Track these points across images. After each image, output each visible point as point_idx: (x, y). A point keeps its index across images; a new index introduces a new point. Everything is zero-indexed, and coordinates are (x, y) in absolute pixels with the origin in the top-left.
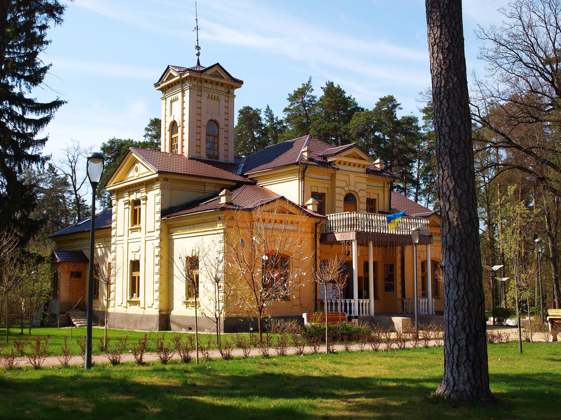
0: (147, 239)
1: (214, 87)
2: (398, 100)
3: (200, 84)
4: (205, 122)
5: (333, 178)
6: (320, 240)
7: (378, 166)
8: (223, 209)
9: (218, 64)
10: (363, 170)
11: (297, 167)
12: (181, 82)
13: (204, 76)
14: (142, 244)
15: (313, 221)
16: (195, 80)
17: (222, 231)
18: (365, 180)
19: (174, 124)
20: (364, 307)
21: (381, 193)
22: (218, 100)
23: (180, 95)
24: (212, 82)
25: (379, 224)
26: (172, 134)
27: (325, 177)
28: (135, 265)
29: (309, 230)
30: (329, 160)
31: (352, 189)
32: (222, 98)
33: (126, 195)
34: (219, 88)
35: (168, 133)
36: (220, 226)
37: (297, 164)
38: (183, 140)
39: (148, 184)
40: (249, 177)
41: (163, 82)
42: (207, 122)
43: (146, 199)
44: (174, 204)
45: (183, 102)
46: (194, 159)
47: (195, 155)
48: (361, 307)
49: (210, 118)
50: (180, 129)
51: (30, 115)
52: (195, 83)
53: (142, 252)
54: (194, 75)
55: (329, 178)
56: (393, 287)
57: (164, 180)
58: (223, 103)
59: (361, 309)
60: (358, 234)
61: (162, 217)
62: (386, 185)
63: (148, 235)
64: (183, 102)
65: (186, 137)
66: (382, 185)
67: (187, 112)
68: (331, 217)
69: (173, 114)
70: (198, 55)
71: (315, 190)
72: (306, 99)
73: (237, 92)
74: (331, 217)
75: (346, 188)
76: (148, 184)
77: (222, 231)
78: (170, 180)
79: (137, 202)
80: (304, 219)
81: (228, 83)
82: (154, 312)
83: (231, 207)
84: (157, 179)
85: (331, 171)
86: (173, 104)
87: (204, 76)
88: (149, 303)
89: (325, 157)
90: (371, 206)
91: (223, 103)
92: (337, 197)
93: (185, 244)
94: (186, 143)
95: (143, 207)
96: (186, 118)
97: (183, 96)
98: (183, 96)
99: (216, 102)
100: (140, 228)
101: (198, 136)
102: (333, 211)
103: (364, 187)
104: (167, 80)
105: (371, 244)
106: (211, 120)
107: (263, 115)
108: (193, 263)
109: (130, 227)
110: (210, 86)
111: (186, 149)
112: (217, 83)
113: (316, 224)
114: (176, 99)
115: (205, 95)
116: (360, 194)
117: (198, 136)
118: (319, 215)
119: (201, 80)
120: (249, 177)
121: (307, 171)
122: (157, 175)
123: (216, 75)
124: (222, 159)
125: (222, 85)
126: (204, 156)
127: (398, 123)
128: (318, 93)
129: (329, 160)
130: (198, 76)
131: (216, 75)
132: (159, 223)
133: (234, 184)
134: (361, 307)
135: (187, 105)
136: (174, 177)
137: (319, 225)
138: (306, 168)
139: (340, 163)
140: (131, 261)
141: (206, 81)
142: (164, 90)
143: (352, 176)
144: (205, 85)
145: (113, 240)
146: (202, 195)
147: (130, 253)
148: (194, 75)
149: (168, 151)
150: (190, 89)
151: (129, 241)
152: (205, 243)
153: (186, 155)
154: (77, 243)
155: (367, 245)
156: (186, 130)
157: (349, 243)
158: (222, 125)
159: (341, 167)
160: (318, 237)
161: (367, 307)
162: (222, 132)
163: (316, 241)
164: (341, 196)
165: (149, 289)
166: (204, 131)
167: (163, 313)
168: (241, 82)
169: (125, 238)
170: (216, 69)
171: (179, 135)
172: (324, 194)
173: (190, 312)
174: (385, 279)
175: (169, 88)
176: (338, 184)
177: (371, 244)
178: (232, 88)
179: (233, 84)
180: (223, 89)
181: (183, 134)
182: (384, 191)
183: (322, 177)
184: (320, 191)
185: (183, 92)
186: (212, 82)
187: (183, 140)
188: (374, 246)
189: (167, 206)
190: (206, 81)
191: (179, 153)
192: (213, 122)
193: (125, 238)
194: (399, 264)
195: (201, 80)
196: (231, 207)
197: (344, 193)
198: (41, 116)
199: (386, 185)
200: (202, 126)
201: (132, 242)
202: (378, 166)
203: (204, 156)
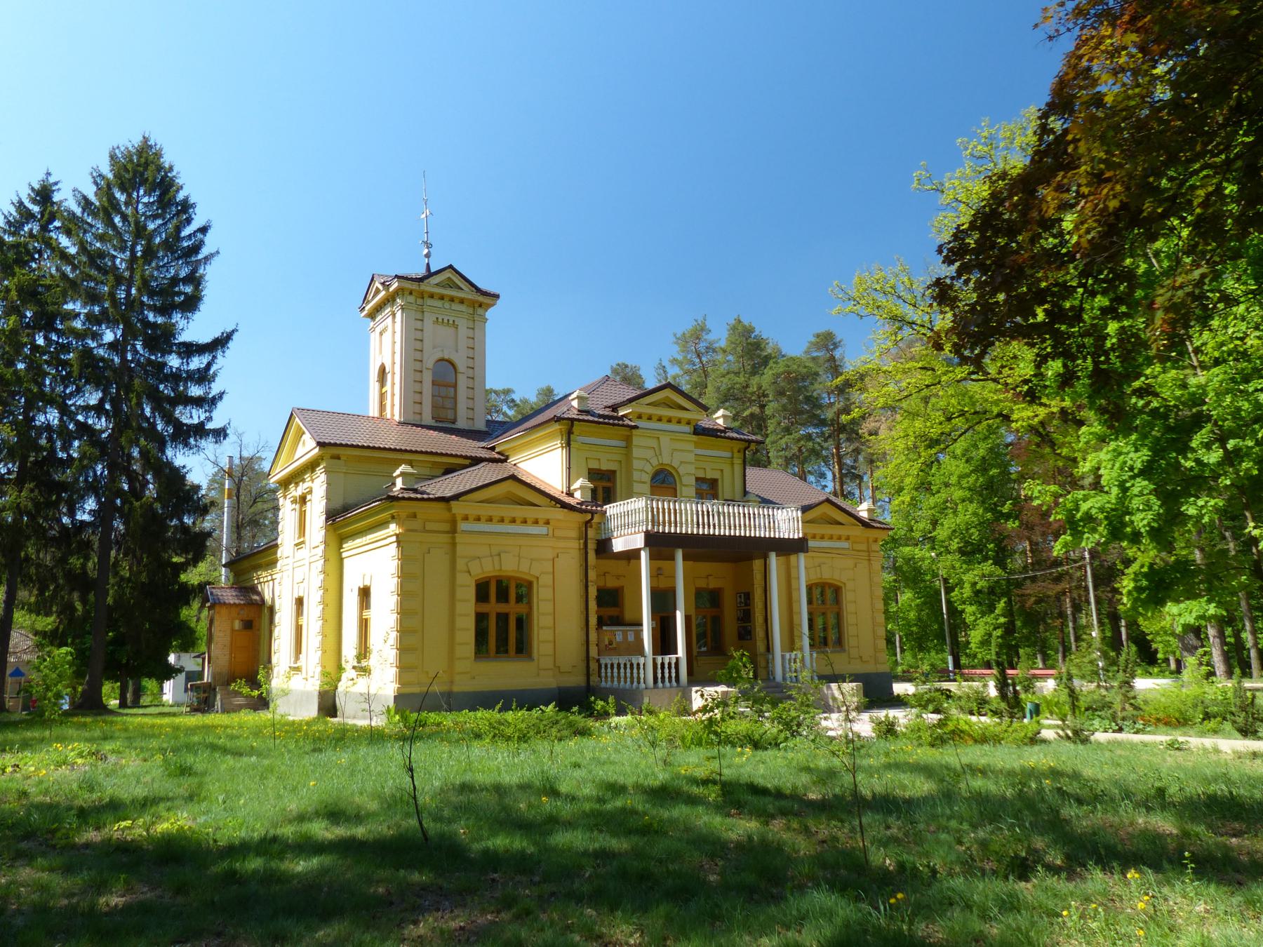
1: (447, 305)
2: (839, 335)
3: (420, 301)
4: (430, 363)
5: (628, 446)
7: (720, 421)
9: (451, 267)
10: (688, 429)
12: (389, 300)
18: (691, 447)
20: (666, 671)
24: (442, 298)
25: (689, 516)
30: (621, 414)
31: (666, 460)
32: (463, 324)
34: (456, 306)
36: (393, 528)
38: (393, 395)
41: (369, 302)
47: (411, 419)
48: (659, 671)
49: (438, 355)
52: (411, 299)
54: (408, 285)
55: (623, 444)
58: (463, 331)
59: (659, 675)
73: (490, 313)
75: (655, 462)
76: (311, 466)
77: (394, 539)
78: (343, 458)
83: (419, 496)
88: (310, 674)
91: (463, 331)
97: (394, 322)
98: (394, 322)
99: (451, 330)
101: (417, 387)
103: (691, 457)
105: (679, 554)
106: (442, 360)
110: (439, 303)
112: (452, 300)
116: (682, 470)
117: (417, 387)
123: (450, 284)
124: (461, 424)
125: (462, 301)
126: (428, 419)
128: (719, 335)
130: (414, 286)
131: (450, 284)
133: (467, 462)
134: (659, 671)
138: (572, 425)
139: (640, 417)
141: (432, 296)
143: (665, 440)
144: (429, 302)
147: (296, 586)
150: (402, 309)
155: (672, 558)
158: (461, 367)
161: (673, 671)
162: (462, 382)
163: (586, 553)
164: (644, 475)
166: (428, 378)
168: (497, 296)
170: (447, 274)
172: (614, 472)
176: (636, 452)
177: (679, 554)
178: (480, 306)
179: (481, 299)
180: (463, 308)
181: (393, 384)
183: (608, 442)
184: (605, 466)
185: (394, 315)
186: (442, 298)
187: (393, 395)
188: (685, 559)
189: (338, 503)
190: (432, 296)
195: (422, 295)
197: (650, 470)
199: (736, 454)
202: (720, 421)
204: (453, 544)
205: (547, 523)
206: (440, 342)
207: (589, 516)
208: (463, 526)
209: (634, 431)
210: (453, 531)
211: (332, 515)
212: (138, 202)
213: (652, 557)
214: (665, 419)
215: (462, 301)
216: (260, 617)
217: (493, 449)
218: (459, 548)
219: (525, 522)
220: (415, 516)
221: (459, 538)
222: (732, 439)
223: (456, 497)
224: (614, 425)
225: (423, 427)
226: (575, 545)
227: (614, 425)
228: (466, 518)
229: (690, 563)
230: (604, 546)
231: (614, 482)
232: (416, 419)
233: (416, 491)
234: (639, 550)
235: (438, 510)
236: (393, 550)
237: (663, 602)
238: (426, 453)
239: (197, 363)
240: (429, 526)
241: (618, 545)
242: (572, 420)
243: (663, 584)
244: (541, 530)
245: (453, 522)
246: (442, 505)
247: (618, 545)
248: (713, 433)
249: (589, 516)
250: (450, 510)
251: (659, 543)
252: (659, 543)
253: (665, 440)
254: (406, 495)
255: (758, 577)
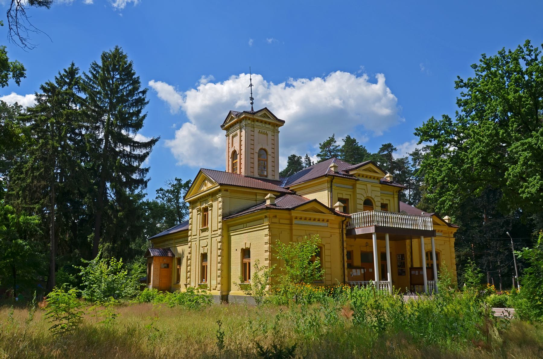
0: (201, 239)
1: (264, 125)
3: (253, 123)
5: (354, 187)
6: (346, 234)
7: (389, 179)
8: (267, 208)
9: (266, 108)
11: (326, 178)
13: (255, 117)
14: (209, 241)
15: (340, 219)
16: (249, 119)
17: (268, 227)
18: (379, 189)
19: (234, 152)
21: (391, 199)
22: (267, 135)
23: (238, 131)
24: (262, 122)
25: (395, 221)
26: (233, 160)
27: (348, 187)
28: (204, 257)
29: (337, 226)
32: (270, 133)
33: (198, 204)
34: (267, 126)
35: (230, 160)
37: (326, 176)
38: (241, 164)
39: (213, 195)
40: (290, 189)
42: (258, 150)
43: (212, 206)
44: (232, 209)
45: (241, 136)
46: (249, 177)
50: (238, 156)
51: (137, 152)
53: (209, 247)
54: (248, 116)
55: (351, 187)
56: (405, 272)
57: (225, 191)
60: (377, 228)
61: (223, 218)
62: (395, 193)
63: (213, 233)
64: (241, 136)
65: (243, 161)
66: (392, 193)
67: (243, 143)
68: (353, 215)
69: (234, 145)
70: (252, 103)
71: (340, 196)
72: (331, 148)
73: (280, 129)
74: (353, 215)
76: (213, 195)
79: (206, 210)
80: (332, 217)
81: (273, 122)
82: (218, 293)
83: (274, 207)
84: (219, 191)
85: (353, 182)
86: (234, 139)
87: (255, 117)
89: (347, 171)
90: (384, 207)
92: (358, 201)
93: (239, 240)
94: (243, 166)
95: (210, 212)
96: (243, 148)
97: (241, 132)
99: (265, 136)
100: (207, 229)
102: (355, 211)
104: (230, 121)
106: (261, 149)
107: (303, 160)
108: (246, 253)
109: (201, 228)
110: (260, 124)
111: (243, 170)
112: (266, 122)
113: (343, 222)
114: (236, 135)
115: (257, 130)
116: (376, 200)
118: (343, 214)
119: (253, 120)
120: (290, 189)
121: (334, 181)
122: (219, 187)
124: (270, 177)
125: (270, 123)
127: (394, 162)
129: (351, 173)
130: (251, 116)
131: (265, 116)
132: (221, 224)
133: (279, 194)
135: (243, 138)
136: (232, 188)
137: (345, 222)
138: (334, 178)
139: (359, 176)
140: (202, 254)
141: (258, 121)
142: (227, 129)
144: (257, 123)
145: (189, 239)
146: (254, 202)
147: (201, 248)
148: (248, 116)
149: (230, 171)
151: (201, 239)
152: (256, 240)
153: (243, 174)
154: (167, 243)
156: (243, 157)
157: (368, 236)
159: (360, 178)
160: (345, 232)
162: (270, 159)
163: (343, 235)
165: (214, 275)
167: (224, 294)
169: (197, 237)
171: (238, 160)
173: (241, 293)
174: (398, 266)
175: (231, 127)
176: (358, 191)
179: (278, 123)
180: (270, 126)
181: (241, 159)
182: (394, 197)
184: (345, 197)
186: (262, 122)
187: (241, 164)
189: (227, 211)
190: (258, 121)
191: (238, 173)
192: (263, 151)
193: (197, 237)
194: (408, 254)
196: (274, 207)
197: (363, 199)
198: (144, 151)
199: (395, 193)
200: (255, 153)
201: (202, 238)
202: (389, 179)
203: (256, 175)
204: (291, 230)
205: (328, 221)
206: (261, 142)
207: (344, 219)
208: (294, 221)
209: (358, 182)
210: (291, 224)
211: (226, 217)
212: (113, 77)
213: (378, 238)
214: (372, 178)
215: (270, 123)
216: (172, 262)
217: (288, 189)
218: (294, 232)
219: (319, 220)
220: (275, 217)
221: (294, 227)
222: (395, 186)
223: (293, 209)
224: (350, 179)
225: (253, 178)
226: (338, 231)
227: (350, 179)
228: (296, 218)
229: (379, 240)
230: (350, 233)
231: (348, 204)
232: (250, 174)
233: (275, 205)
234: (371, 234)
235: (286, 214)
236: (267, 231)
237: (382, 257)
238: (263, 189)
239: (138, 152)
240: (281, 221)
241: (358, 232)
242: (334, 176)
243: (383, 250)
244: (325, 224)
245: (291, 220)
246: (287, 212)
247: (358, 232)
248: (385, 183)
249: (344, 219)
250: (290, 214)
251: (381, 231)
252: (381, 231)
253: (369, 186)
254: (272, 207)
255: (408, 247)
